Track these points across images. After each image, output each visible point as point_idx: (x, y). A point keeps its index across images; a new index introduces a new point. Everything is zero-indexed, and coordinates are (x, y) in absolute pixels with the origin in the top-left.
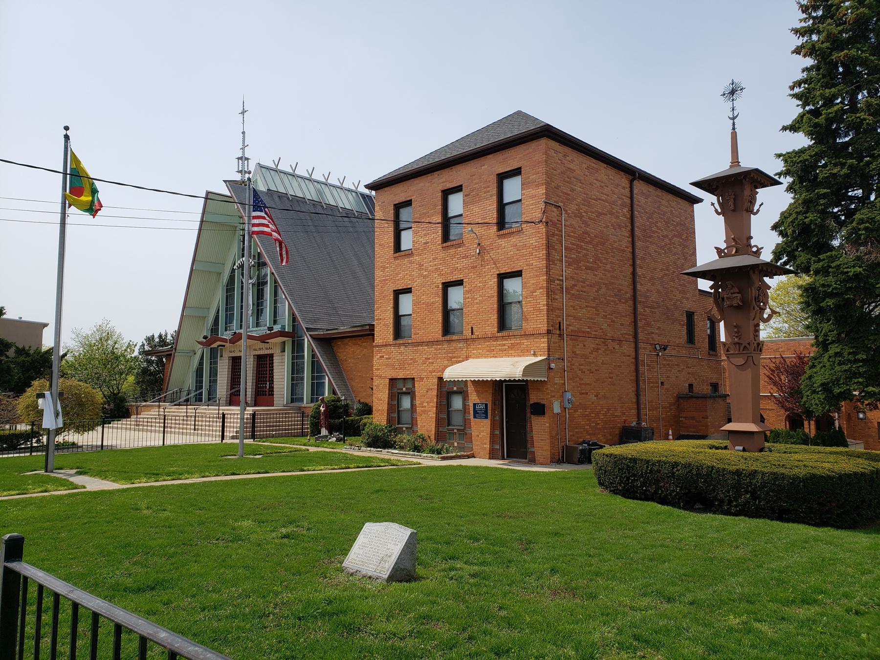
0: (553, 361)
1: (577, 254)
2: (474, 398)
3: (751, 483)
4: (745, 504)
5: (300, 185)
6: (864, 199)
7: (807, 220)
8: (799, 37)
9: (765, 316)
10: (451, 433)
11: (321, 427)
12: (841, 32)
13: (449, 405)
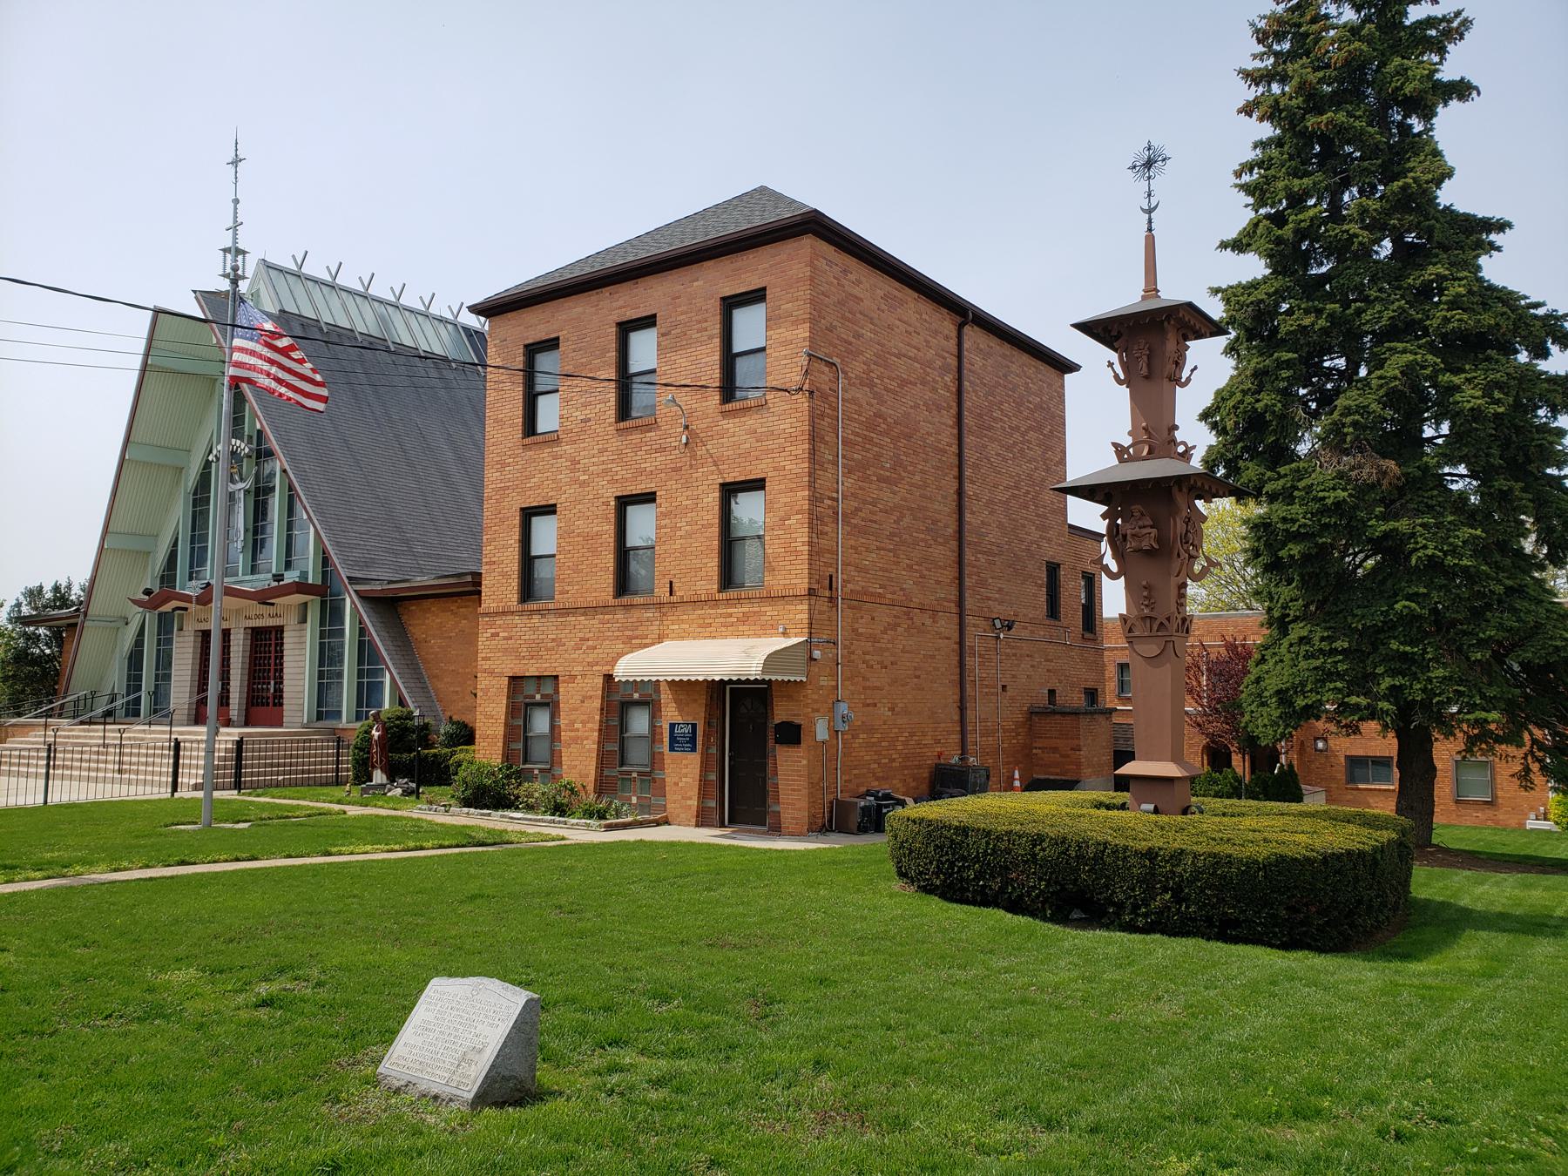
0: (818, 646)
1: (864, 454)
2: (671, 713)
3: (1174, 873)
4: (1162, 913)
5: (344, 307)
6: (1349, 375)
7: (1259, 406)
8: (1250, 86)
9: (1197, 568)
10: (626, 778)
11: (374, 767)
12: (1321, 81)
13: (623, 726)
